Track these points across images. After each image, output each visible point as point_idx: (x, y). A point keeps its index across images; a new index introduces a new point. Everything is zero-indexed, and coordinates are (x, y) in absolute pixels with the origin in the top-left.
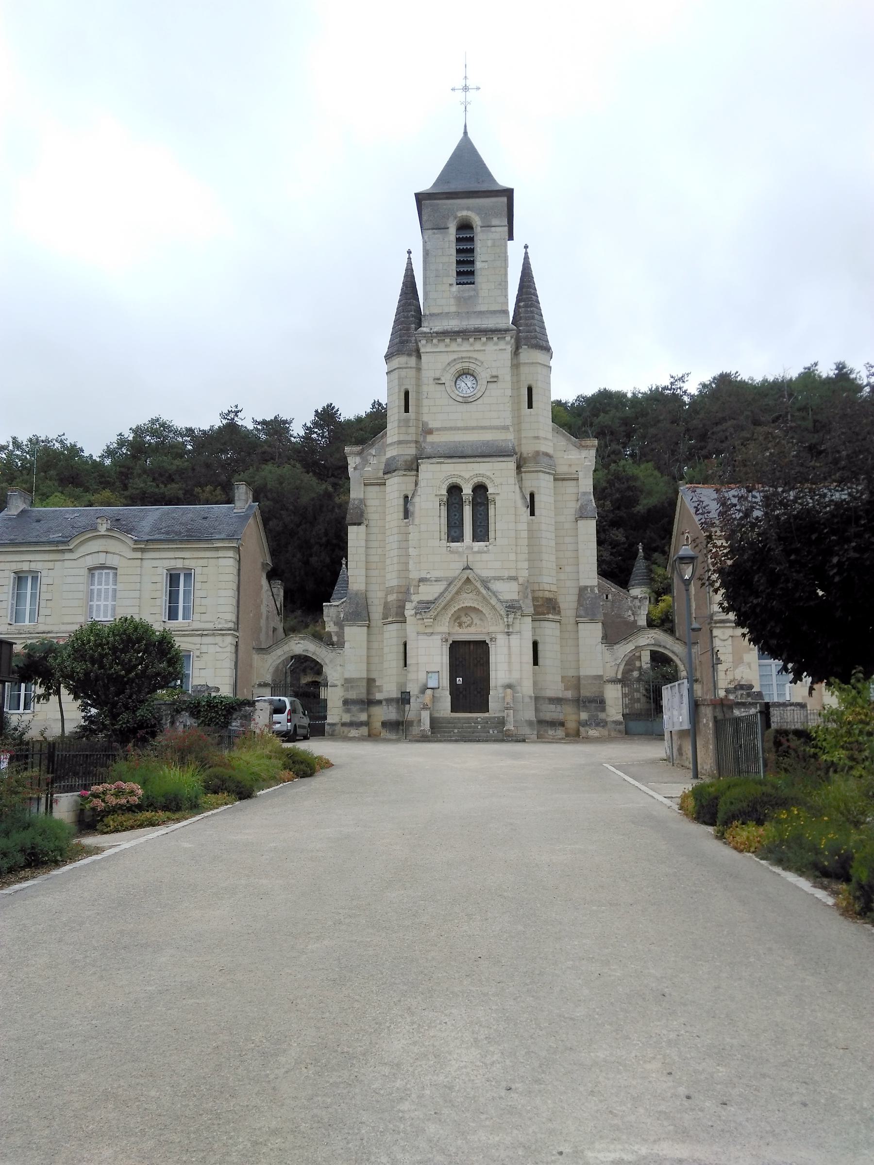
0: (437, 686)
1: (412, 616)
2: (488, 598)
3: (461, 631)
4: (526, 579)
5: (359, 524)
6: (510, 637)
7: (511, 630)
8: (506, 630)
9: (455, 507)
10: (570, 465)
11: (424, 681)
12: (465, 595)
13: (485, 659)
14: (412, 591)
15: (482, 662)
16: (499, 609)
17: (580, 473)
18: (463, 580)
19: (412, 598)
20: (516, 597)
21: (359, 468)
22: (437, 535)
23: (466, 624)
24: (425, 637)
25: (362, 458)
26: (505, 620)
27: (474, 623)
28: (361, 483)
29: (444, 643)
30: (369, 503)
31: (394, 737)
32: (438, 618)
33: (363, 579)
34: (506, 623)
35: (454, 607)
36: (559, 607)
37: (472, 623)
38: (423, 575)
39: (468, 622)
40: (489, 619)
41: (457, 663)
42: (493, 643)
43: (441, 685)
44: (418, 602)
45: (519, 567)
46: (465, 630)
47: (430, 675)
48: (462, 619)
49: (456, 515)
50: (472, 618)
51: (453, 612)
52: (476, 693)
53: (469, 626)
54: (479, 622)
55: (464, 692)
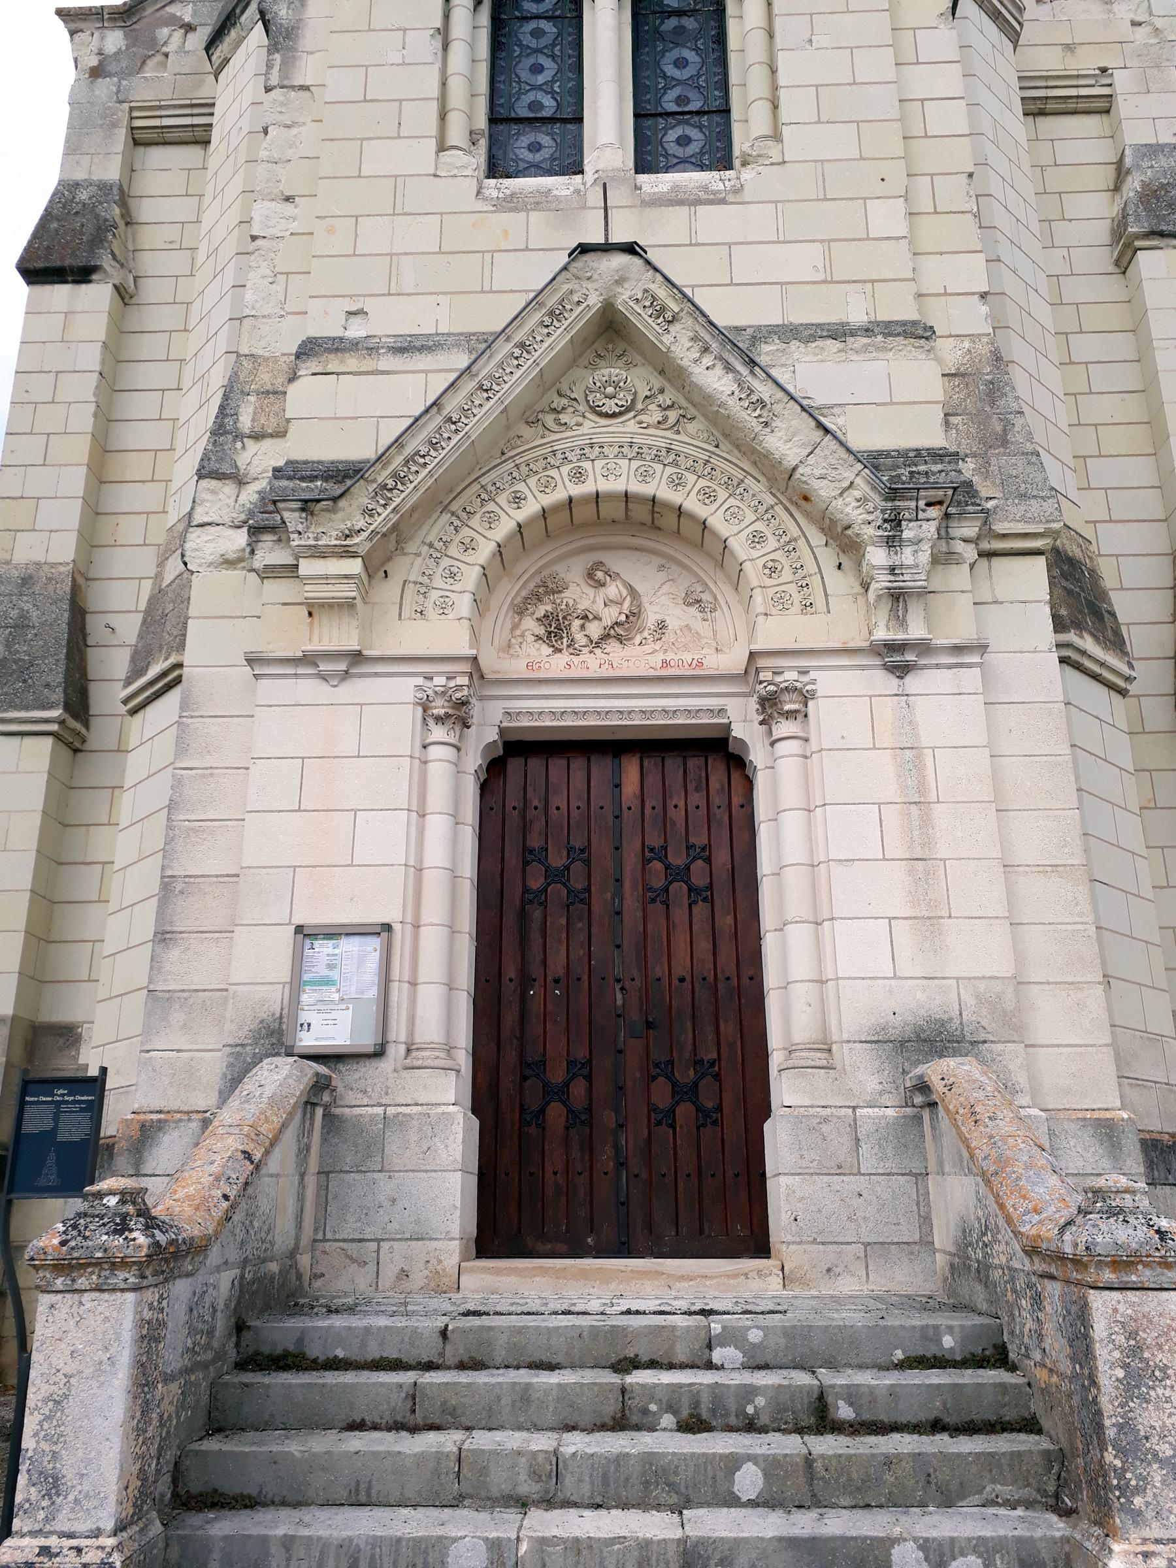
0: (367, 1041)
1: (229, 563)
2: (749, 419)
3: (558, 664)
4: (983, 348)
5: (83, 275)
6: (913, 682)
7: (916, 630)
8: (881, 634)
9: (537, 33)
10: (1069, 48)
11: (273, 999)
12: (591, 426)
13: (721, 857)
14: (246, 422)
15: (699, 877)
16: (824, 490)
17: (1119, 77)
18: (576, 320)
19: (242, 460)
20: (935, 438)
21: (113, 67)
22: (426, 117)
23: (594, 629)
24: (308, 689)
25: (133, 39)
26: (877, 556)
27: (651, 618)
28: (114, 125)
29: (439, 733)
30: (146, 211)
31: (172, 1357)
32: (405, 568)
33: (70, 515)
34: (882, 582)
35: (518, 500)
36: (1113, 615)
37: (634, 615)
38: (328, 326)
39: (610, 615)
40: (753, 573)
41: (536, 883)
42: (784, 728)
43: (398, 1031)
44: (278, 472)
45: (931, 285)
46: (592, 663)
47: (323, 949)
48: (568, 596)
49: (537, 69)
50: (633, 591)
51: (505, 528)
52: (661, 1094)
53: (619, 633)
54: (678, 616)
55: (578, 1090)
